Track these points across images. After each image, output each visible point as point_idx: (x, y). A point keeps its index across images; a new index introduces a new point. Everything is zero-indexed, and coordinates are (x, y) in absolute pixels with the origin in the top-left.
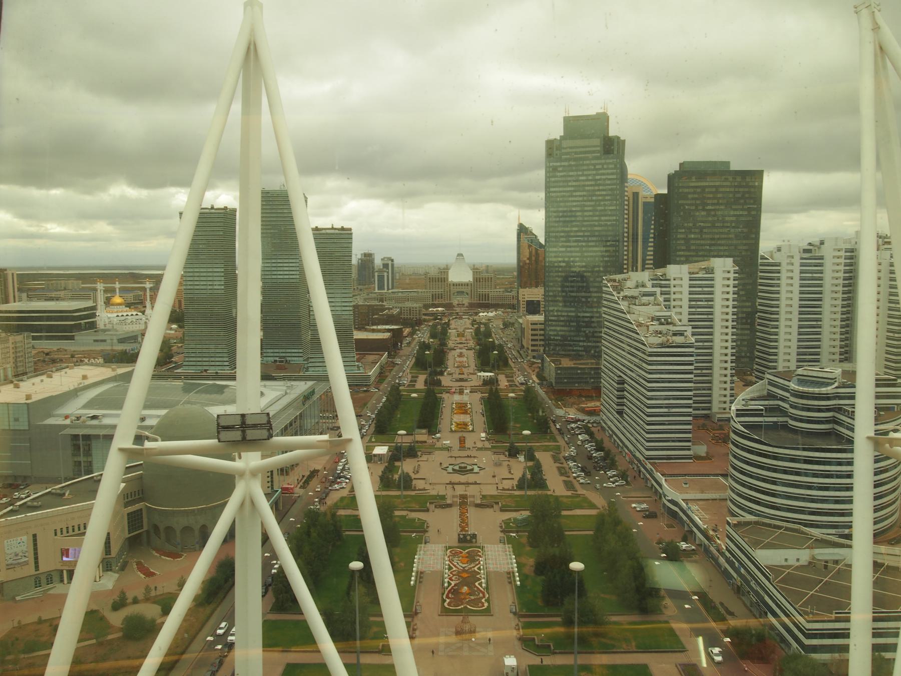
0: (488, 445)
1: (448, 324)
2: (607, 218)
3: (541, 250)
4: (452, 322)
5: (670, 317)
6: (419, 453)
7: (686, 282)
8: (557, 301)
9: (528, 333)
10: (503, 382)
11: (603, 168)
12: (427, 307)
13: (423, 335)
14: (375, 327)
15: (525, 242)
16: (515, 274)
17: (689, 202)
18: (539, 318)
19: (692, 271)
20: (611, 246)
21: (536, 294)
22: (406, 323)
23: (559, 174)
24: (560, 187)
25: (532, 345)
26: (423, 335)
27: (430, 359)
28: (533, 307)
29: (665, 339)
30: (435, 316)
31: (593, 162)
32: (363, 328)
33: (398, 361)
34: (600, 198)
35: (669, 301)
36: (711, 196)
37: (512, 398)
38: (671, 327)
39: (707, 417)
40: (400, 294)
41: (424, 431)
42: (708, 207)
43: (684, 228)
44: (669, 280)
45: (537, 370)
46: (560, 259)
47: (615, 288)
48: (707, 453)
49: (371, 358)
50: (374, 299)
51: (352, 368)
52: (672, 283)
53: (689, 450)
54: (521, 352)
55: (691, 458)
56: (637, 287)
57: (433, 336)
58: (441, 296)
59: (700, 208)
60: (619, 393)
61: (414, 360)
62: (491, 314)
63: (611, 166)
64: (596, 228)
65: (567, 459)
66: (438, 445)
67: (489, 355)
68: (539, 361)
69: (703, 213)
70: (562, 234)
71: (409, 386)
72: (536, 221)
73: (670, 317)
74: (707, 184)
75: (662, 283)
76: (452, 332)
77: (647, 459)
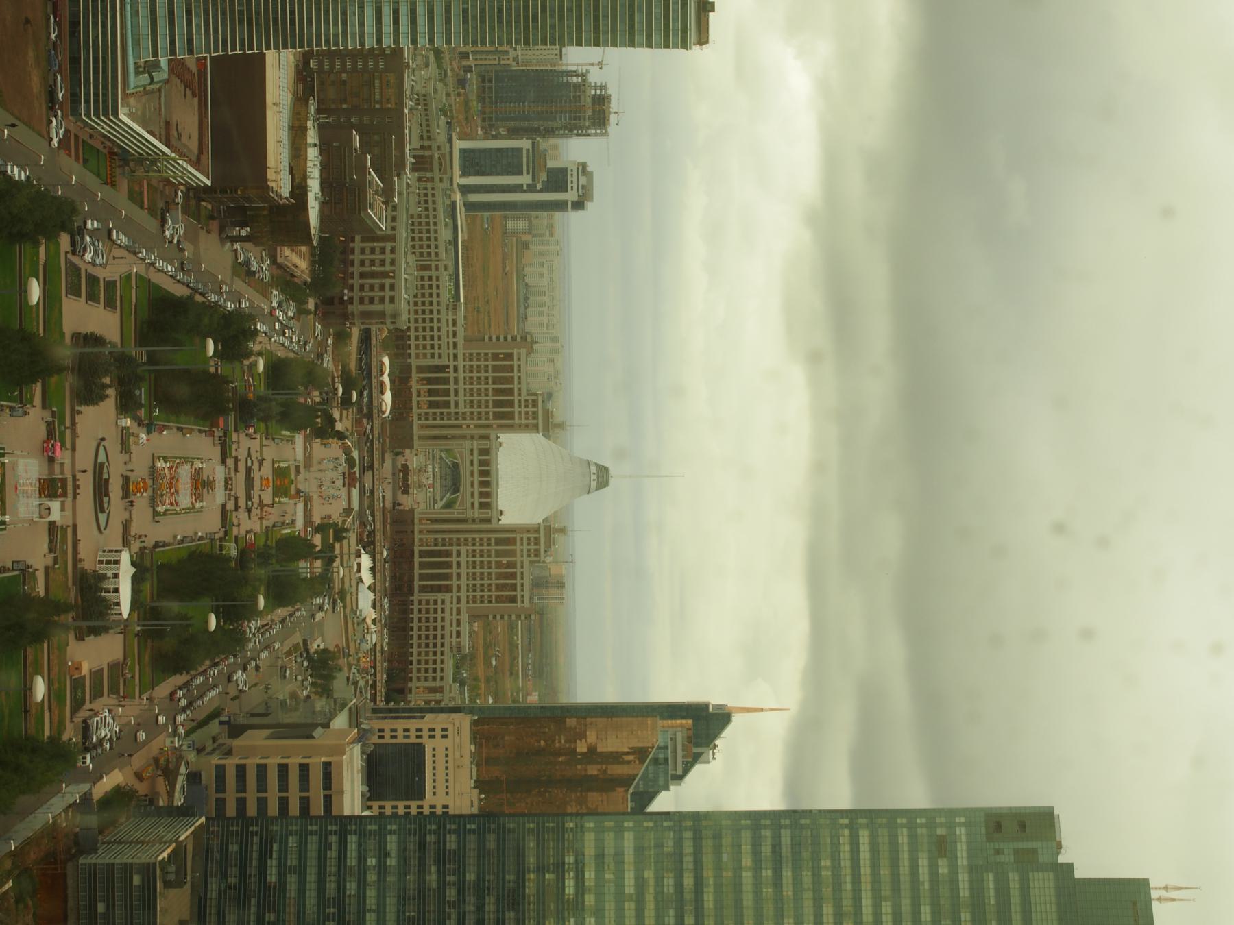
1: (326, 431)
3: (624, 799)
4: (335, 444)
8: (422, 868)
9: (293, 753)
10: (93, 654)
12: (399, 343)
13: (282, 331)
14: (312, 136)
15: (659, 734)
16: (533, 698)
18: (352, 801)
21: (452, 785)
22: (330, 256)
23: (923, 862)
24: (875, 866)
26: (282, 331)
27: (180, 358)
28: (394, 771)
30: (361, 378)
33: (175, 228)
37: (28, 689)
40: (445, 234)
45: (142, 789)
46: (590, 875)
49: (187, 118)
50: (426, 136)
51: (146, 43)
54: (214, 727)
57: (278, 370)
58: (439, 400)
61: (180, 291)
62: (365, 600)
67: (203, 596)
68: (179, 800)
70: (688, 880)
71: (74, 270)
72: (738, 779)
76: (296, 447)
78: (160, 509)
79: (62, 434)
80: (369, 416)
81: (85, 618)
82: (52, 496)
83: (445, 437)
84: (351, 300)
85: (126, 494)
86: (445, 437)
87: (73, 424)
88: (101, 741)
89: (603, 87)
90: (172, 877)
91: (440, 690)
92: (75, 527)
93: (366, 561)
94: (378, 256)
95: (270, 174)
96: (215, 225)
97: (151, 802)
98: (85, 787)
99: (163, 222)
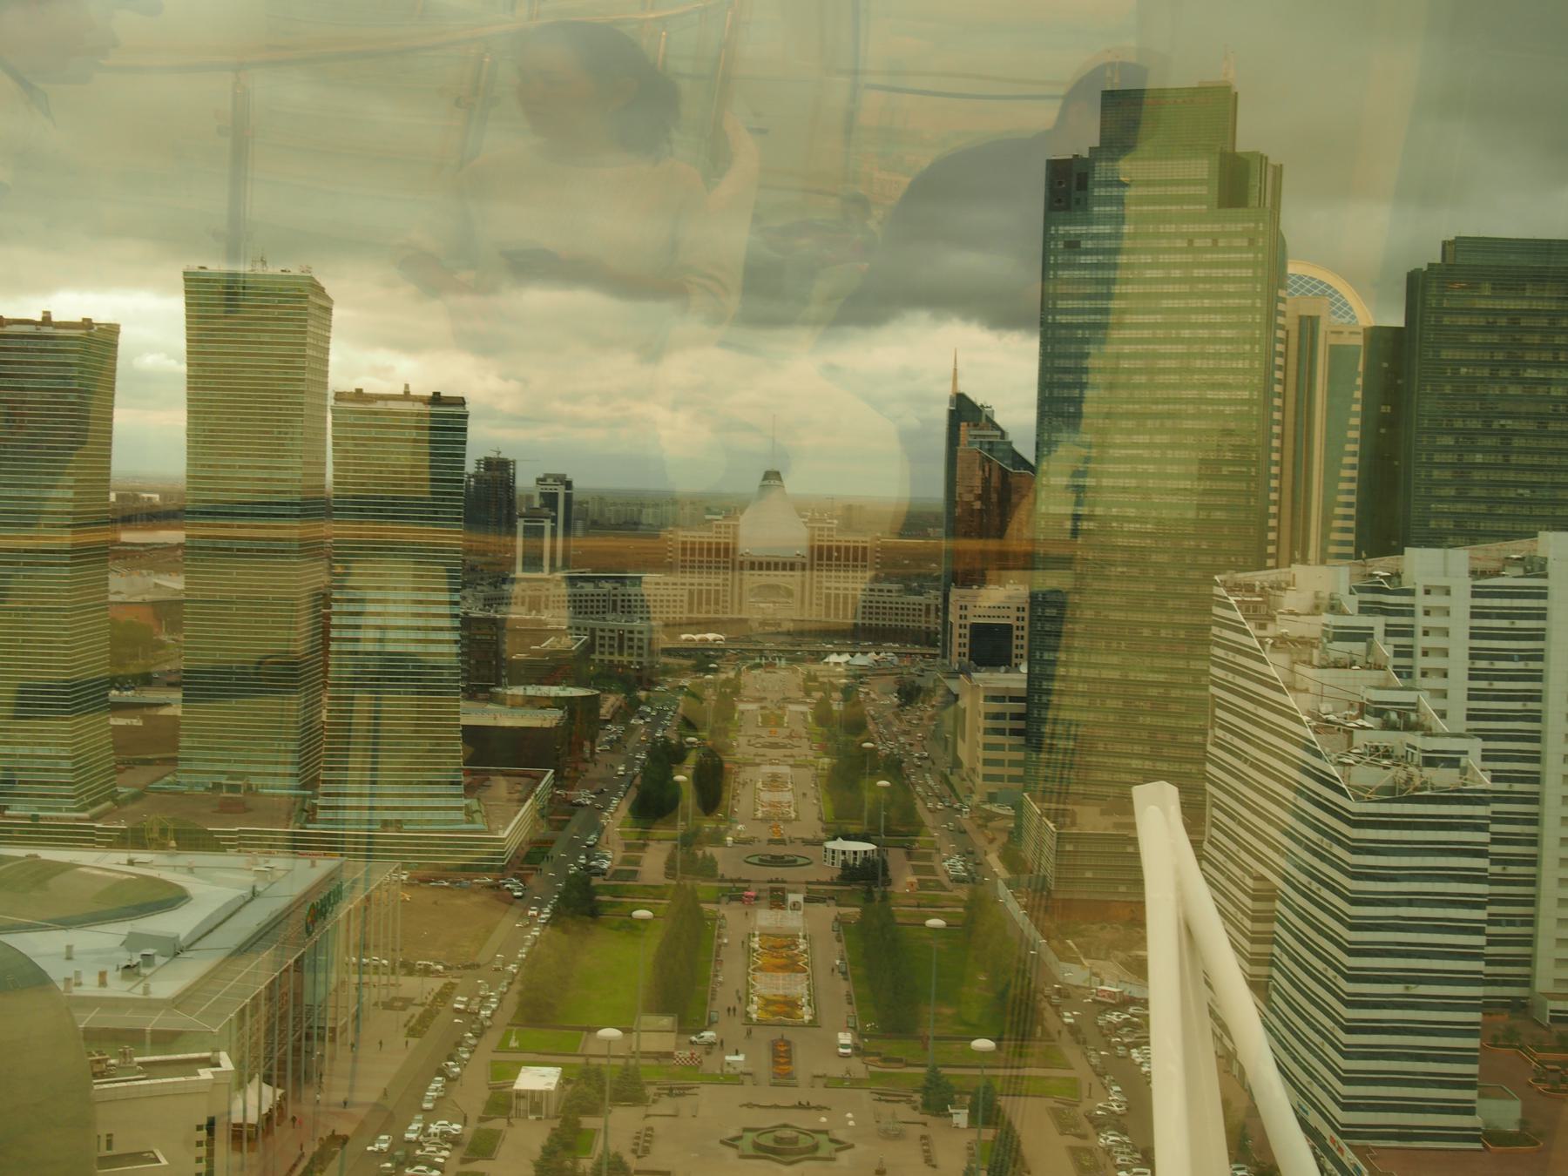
0: (858, 1067)
2: (1223, 395)
4: (744, 679)
5: (1415, 707)
6: (651, 1091)
7: (1461, 602)
11: (1215, 247)
17: (1472, 355)
19: (1480, 566)
20: (1232, 477)
22: (609, 677)
23: (1083, 259)
25: (987, 762)
29: (1403, 775)
31: (1185, 228)
32: (485, 689)
33: (584, 796)
34: (1204, 333)
35: (1410, 655)
36: (1536, 339)
38: (1416, 739)
39: (1519, 1007)
41: (666, 1021)
42: (1531, 373)
43: (1451, 431)
44: (1411, 593)
45: (1002, 838)
47: (1251, 611)
48: (1523, 1123)
52: (1421, 601)
53: (1470, 1111)
54: (954, 779)
55: (1476, 1139)
56: (1316, 610)
59: (1505, 373)
60: (1259, 927)
62: (860, 660)
63: (1238, 242)
64: (1188, 424)
65: (1099, 1125)
66: (710, 1064)
69: (1513, 390)
73: (1415, 707)
74: (1524, 305)
75: (1385, 598)
77: (1343, 1135)
78: (793, 815)
79: (739, 889)
80: (724, 650)
81: (876, 878)
82: (784, 900)
83: (740, 595)
84: (639, 663)
85: (782, 842)
86: (740, 595)
87: (731, 881)
88: (966, 870)
89: (479, 462)
90: (1068, 820)
91: (928, 606)
92: (808, 883)
93: (833, 658)
94: (607, 642)
95: (547, 725)
96: (581, 766)
97: (1011, 833)
98: (1000, 883)
99: (579, 805)
